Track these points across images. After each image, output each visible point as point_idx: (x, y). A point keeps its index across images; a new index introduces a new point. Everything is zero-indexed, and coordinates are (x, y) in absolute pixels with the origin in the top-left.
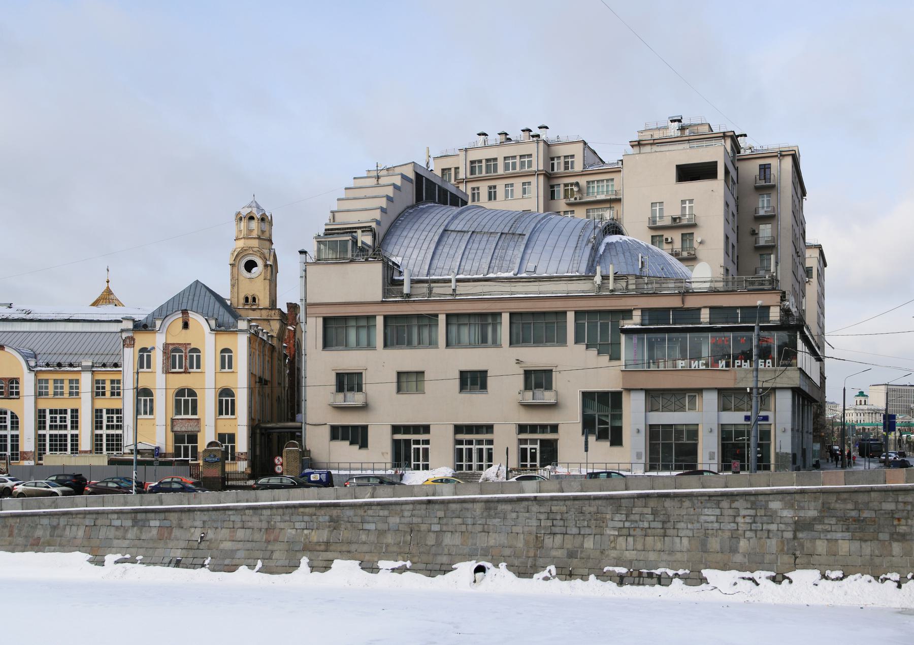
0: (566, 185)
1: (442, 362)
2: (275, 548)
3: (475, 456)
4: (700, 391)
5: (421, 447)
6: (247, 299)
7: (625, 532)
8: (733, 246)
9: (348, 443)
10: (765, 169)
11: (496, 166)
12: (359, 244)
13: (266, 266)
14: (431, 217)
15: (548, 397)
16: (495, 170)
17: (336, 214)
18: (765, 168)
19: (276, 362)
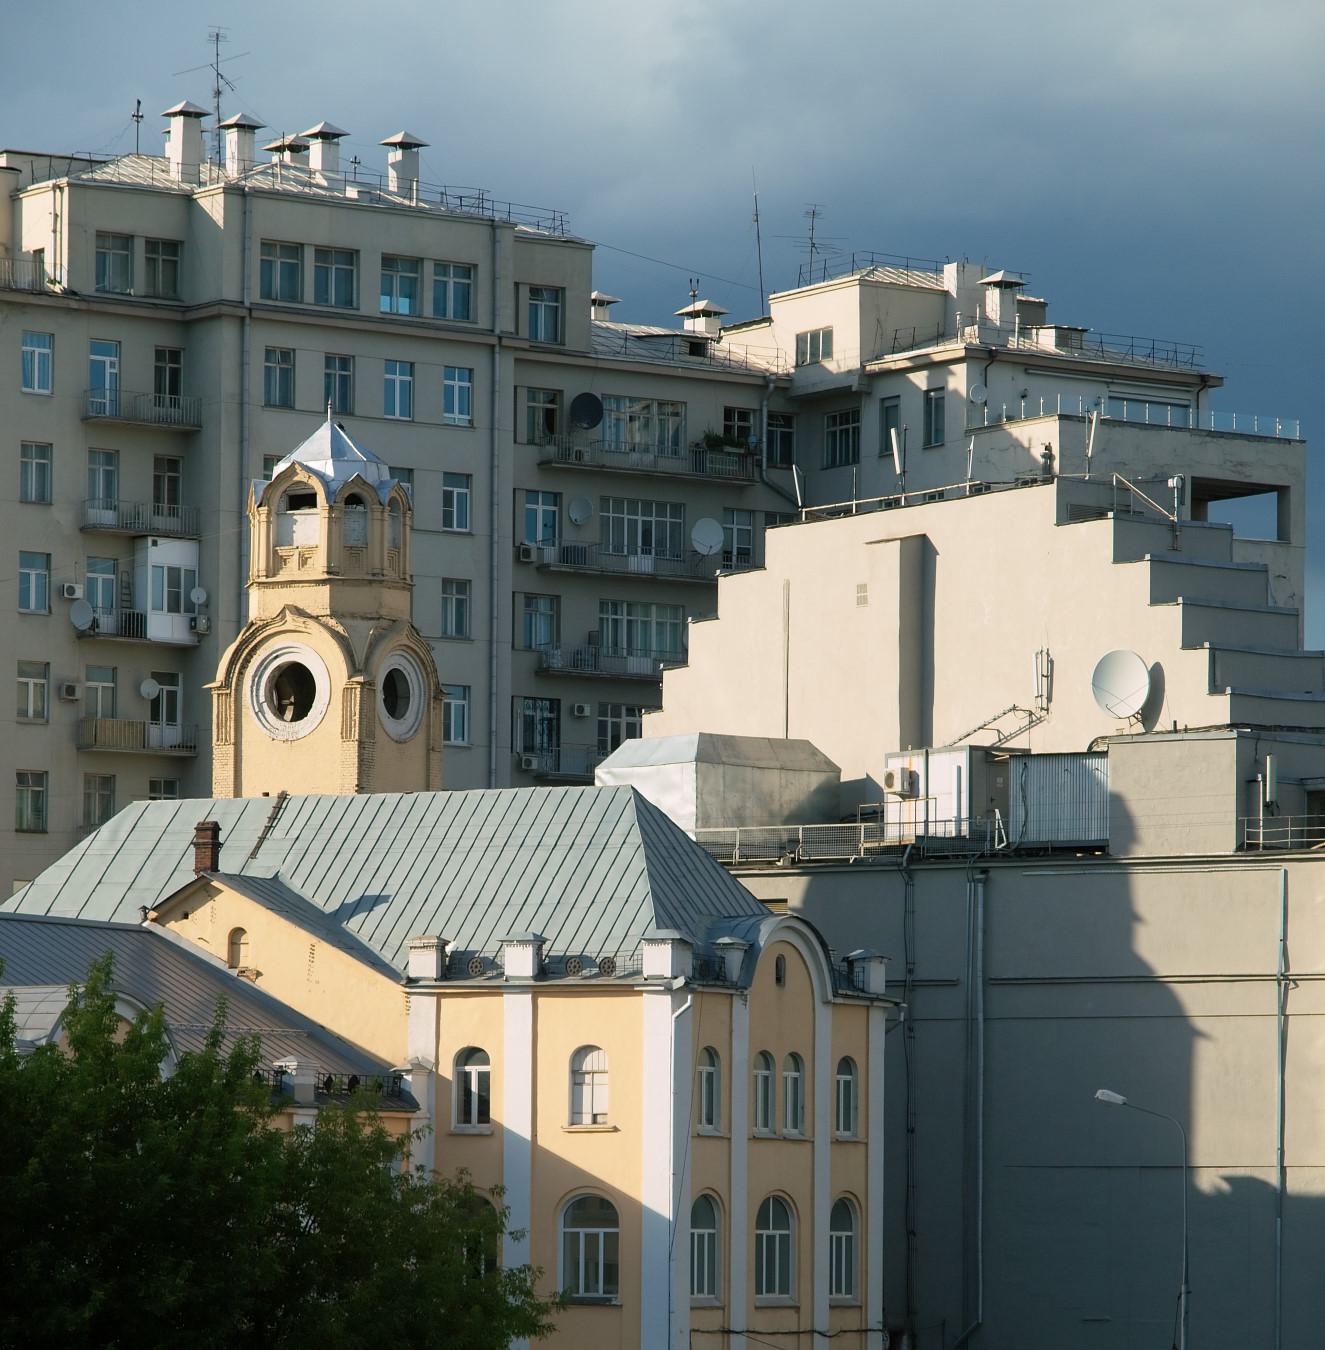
17: (809, 1146)
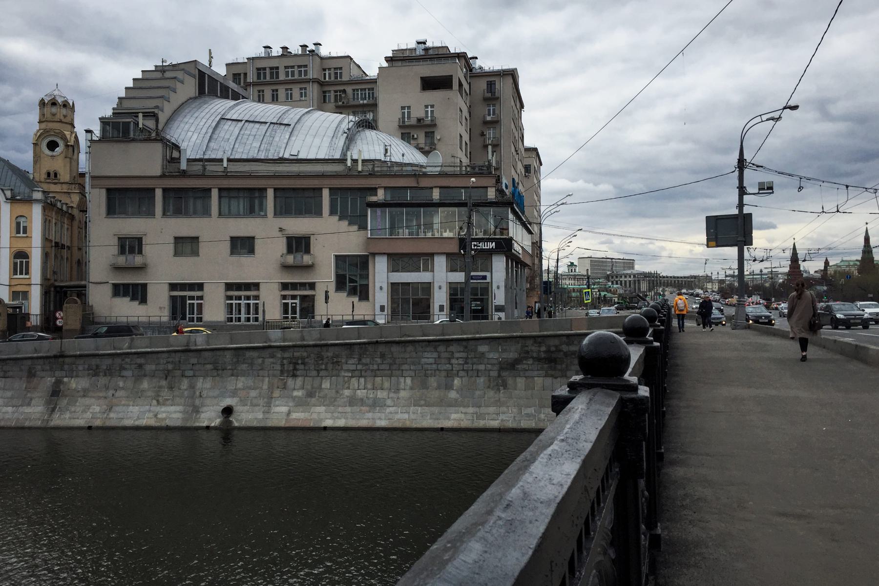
0: (336, 91)
1: (215, 229)
2: (33, 396)
3: (243, 310)
4: (432, 255)
5: (195, 302)
6: (49, 174)
7: (357, 373)
8: (466, 144)
9: (129, 299)
11: (277, 73)
12: (141, 126)
13: (67, 146)
14: (211, 107)
15: (138, 260)
16: (277, 77)
18: (491, 85)
19: (76, 231)
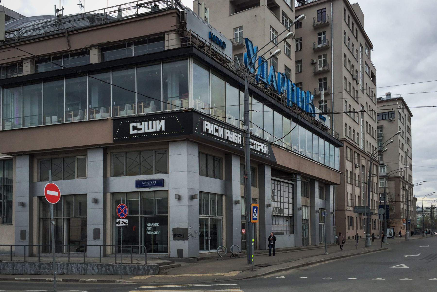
10: (321, 13)
